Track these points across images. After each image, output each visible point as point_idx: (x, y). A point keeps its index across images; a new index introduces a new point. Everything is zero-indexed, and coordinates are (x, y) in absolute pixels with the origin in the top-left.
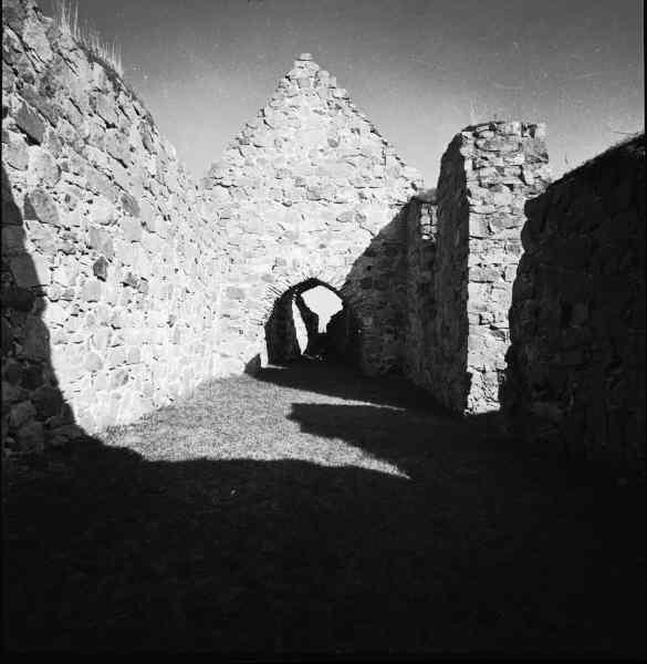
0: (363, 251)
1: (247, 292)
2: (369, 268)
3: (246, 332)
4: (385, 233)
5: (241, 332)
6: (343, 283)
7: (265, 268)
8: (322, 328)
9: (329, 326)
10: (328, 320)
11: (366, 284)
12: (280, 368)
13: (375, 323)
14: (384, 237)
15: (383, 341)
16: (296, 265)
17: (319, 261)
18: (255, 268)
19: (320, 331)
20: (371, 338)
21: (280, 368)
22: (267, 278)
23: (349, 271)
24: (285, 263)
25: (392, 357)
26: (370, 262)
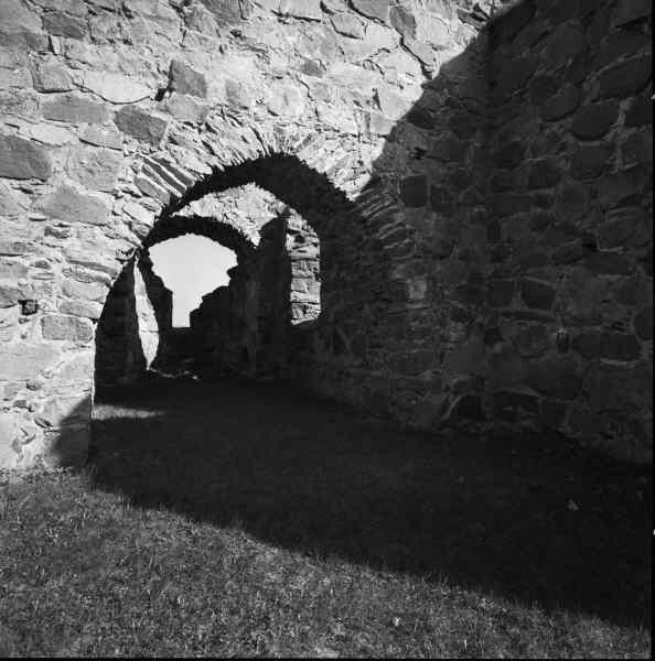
0: (409, 107)
1: (55, 160)
2: (420, 153)
3: (51, 305)
4: (451, 76)
5: (28, 308)
6: (364, 179)
7: (134, 90)
8: (181, 319)
9: (194, 315)
10: (196, 303)
11: (414, 192)
12: (144, 414)
13: (434, 295)
14: (450, 84)
15: (445, 339)
16: (233, 110)
17: (300, 108)
18: (92, 79)
19: (299, 318)
20: (424, 333)
21: (144, 414)
22: (134, 123)
23: (377, 152)
24: (201, 87)
25: (463, 377)
26: (417, 138)
